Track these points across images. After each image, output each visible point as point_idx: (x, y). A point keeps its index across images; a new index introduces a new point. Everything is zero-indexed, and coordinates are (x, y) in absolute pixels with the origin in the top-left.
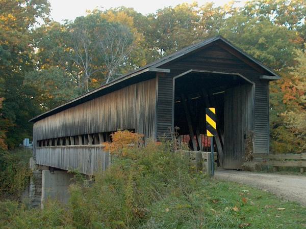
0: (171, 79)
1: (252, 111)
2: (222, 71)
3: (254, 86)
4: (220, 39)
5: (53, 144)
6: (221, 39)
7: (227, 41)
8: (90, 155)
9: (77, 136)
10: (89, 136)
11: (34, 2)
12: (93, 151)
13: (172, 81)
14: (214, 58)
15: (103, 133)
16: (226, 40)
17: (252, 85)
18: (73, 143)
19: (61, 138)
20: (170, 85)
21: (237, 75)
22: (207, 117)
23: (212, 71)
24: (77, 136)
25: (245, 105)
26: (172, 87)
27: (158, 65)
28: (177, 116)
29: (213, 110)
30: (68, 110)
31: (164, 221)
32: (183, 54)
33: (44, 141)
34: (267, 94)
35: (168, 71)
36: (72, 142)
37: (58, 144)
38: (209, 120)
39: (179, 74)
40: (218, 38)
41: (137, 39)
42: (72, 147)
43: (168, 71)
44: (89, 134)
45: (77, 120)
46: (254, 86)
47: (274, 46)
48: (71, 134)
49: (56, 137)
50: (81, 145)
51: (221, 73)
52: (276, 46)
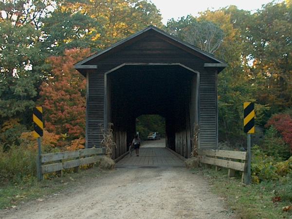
0: (103, 75)
2: (160, 63)
3: (198, 75)
6: (153, 28)
7: (164, 33)
13: (104, 76)
14: (149, 50)
16: (163, 31)
17: (197, 74)
20: (102, 83)
21: (179, 65)
23: (148, 63)
25: (175, 167)
26: (104, 83)
27: (83, 62)
28: (113, 117)
32: (110, 48)
34: (214, 83)
35: (95, 67)
39: (110, 69)
40: (150, 28)
41: (232, 35)
43: (95, 67)
46: (198, 75)
47: (225, 176)
51: (159, 64)
52: (279, 134)
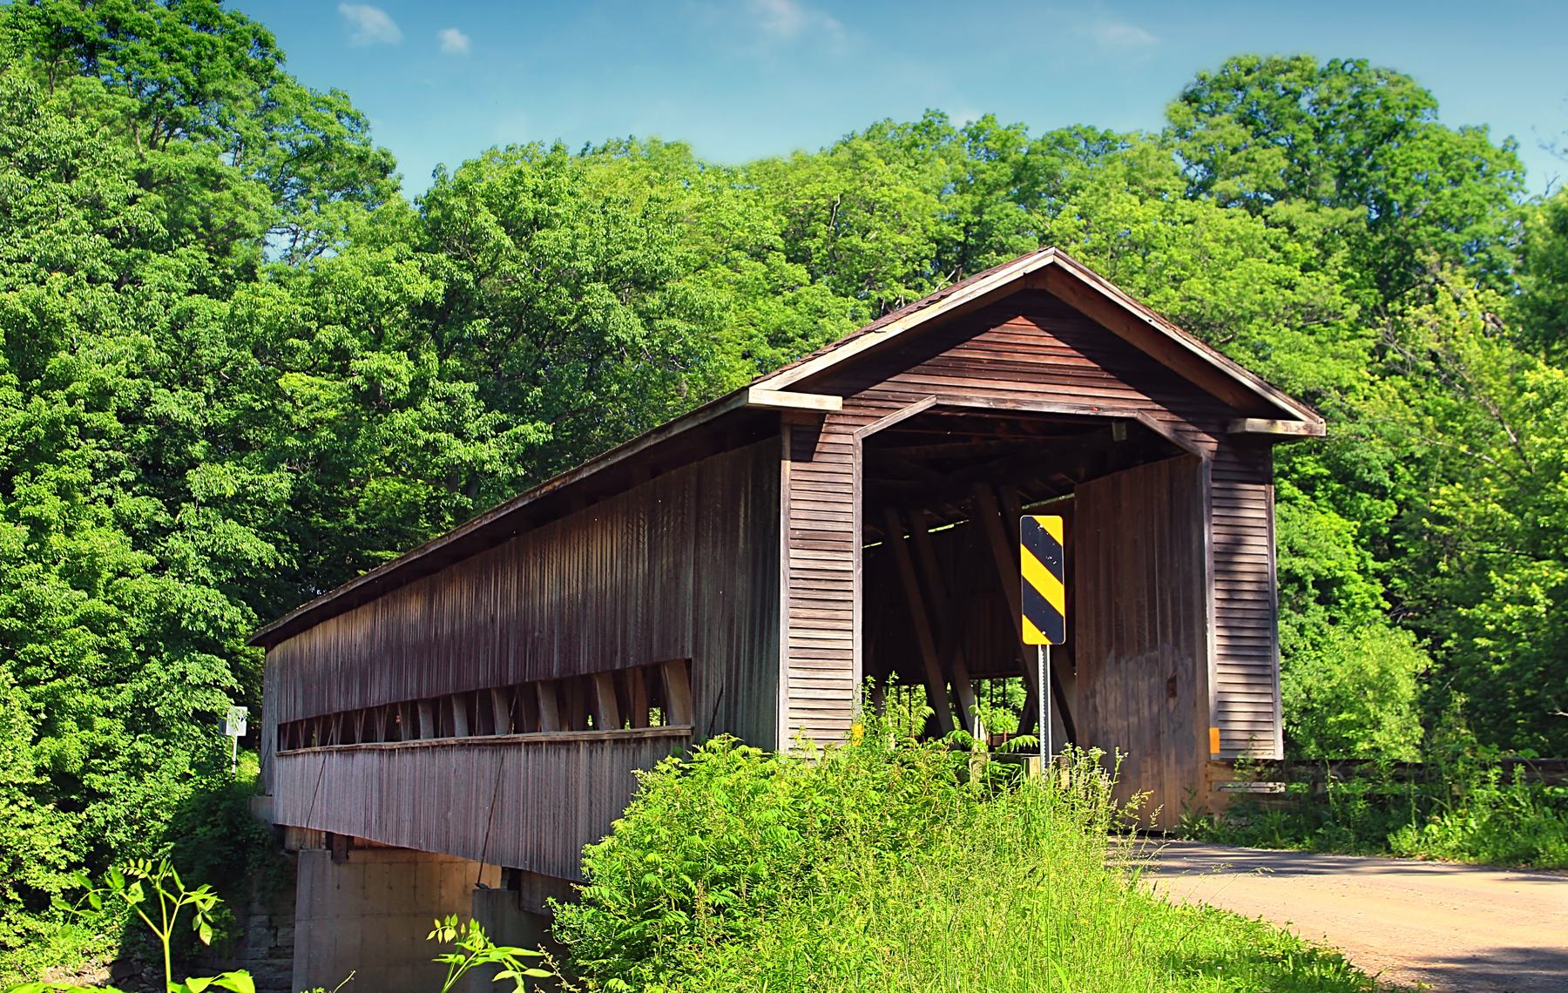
1: (1326, 849)
4: (1053, 265)
5: (347, 738)
8: (500, 775)
9: (447, 700)
10: (494, 695)
11: (2, 131)
12: (511, 757)
15: (556, 681)
18: (431, 729)
19: (318, 718)
22: (1026, 556)
24: (586, 683)
29: (1053, 525)
30: (407, 588)
31: (1393, 484)
33: (310, 722)
36: (424, 723)
37: (308, 745)
38: (1033, 569)
42: (424, 748)
44: (497, 690)
45: (447, 628)
48: (419, 693)
49: (300, 717)
50: (461, 736)
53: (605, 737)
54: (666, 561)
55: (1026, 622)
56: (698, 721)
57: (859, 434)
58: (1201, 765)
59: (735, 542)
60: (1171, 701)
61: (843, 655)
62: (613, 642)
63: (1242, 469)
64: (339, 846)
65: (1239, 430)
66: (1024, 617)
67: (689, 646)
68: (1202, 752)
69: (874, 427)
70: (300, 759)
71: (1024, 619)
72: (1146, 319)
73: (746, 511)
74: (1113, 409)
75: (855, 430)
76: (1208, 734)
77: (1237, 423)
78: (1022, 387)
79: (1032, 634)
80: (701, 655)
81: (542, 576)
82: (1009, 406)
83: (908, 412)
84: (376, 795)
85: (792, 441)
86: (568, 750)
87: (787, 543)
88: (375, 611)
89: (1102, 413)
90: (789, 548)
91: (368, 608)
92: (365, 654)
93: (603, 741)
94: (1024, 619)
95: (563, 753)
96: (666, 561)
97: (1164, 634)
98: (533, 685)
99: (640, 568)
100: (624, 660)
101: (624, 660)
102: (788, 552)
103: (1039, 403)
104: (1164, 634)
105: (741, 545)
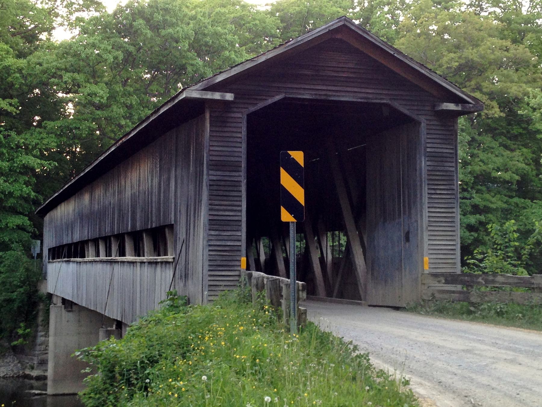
29: (298, 156)
50: (103, 257)
53: (145, 261)
54: (165, 177)
55: (283, 210)
56: (176, 255)
57: (246, 112)
58: (420, 275)
59: (189, 165)
60: (407, 243)
61: (235, 224)
62: (148, 217)
63: (443, 128)
64: (68, 304)
65: (440, 108)
66: (303, 204)
67: (173, 219)
68: (420, 270)
69: (252, 109)
70: (54, 264)
71: (282, 207)
72: (392, 53)
73: (193, 152)
74: (376, 99)
75: (243, 110)
76: (423, 260)
77: (439, 105)
78: (329, 88)
79: (286, 216)
80: (177, 222)
81: (125, 183)
82: (323, 98)
83: (270, 101)
84: (76, 282)
85: (210, 116)
86: (133, 266)
87: (207, 168)
88: (75, 201)
89: (370, 101)
90: (208, 169)
91: (74, 197)
92: (73, 220)
93: (144, 262)
94: (282, 207)
95: (132, 267)
96: (165, 177)
97: (404, 211)
98: (124, 234)
99: (156, 181)
100: (152, 225)
101: (152, 225)
102: (208, 172)
103: (338, 96)
104: (404, 211)
105: (191, 169)
